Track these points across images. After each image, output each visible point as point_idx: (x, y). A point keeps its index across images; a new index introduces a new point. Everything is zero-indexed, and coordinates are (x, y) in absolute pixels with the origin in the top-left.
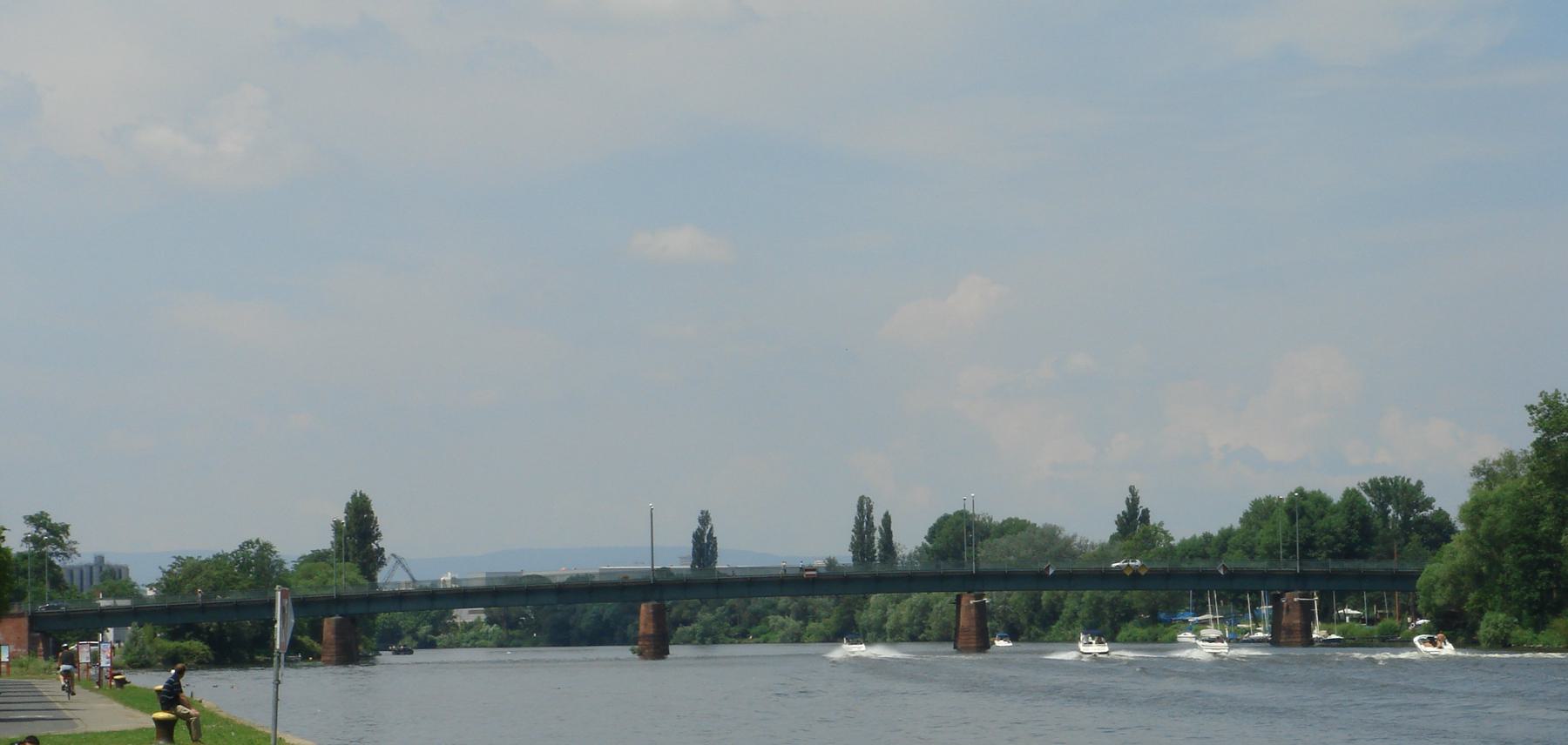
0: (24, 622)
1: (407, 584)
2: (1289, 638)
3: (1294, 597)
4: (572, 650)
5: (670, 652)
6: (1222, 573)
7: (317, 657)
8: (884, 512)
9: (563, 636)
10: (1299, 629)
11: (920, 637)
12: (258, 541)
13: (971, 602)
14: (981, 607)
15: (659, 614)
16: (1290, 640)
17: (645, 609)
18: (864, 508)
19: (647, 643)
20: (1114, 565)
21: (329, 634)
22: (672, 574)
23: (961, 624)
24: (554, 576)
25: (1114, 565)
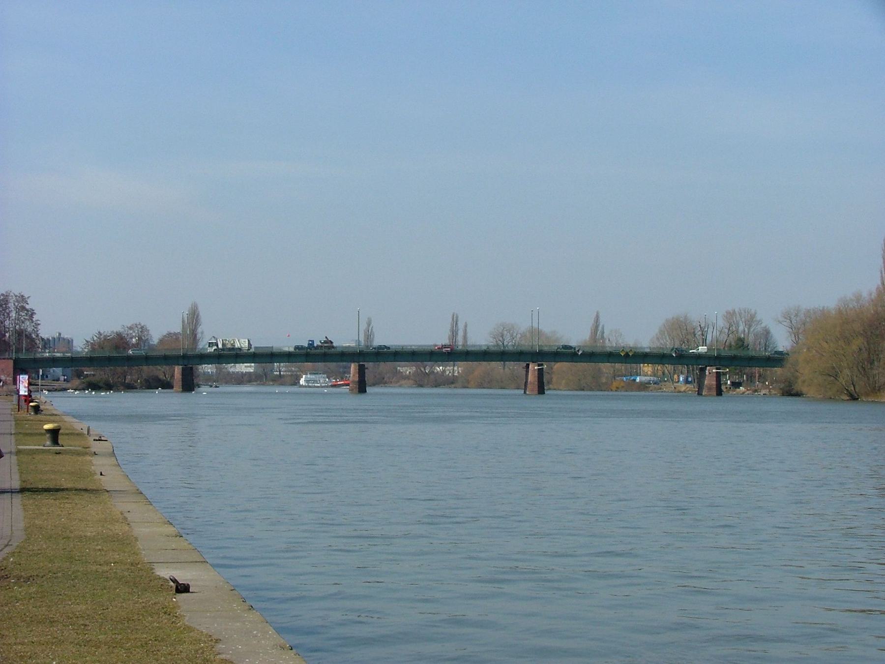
0: (11, 363)
1: (494, 346)
2: (710, 392)
3: (713, 369)
4: (167, 392)
5: (367, 391)
6: (674, 355)
7: (136, 388)
8: (465, 322)
9: (539, 378)
10: (715, 387)
11: (615, 384)
12: (140, 324)
13: (536, 368)
14: (541, 372)
15: (362, 371)
16: (711, 393)
17: (353, 367)
18: (455, 321)
19: (355, 386)
20: (691, 351)
21: (178, 375)
22: (747, 347)
23: (529, 380)
24: (407, 346)
25: (691, 351)
